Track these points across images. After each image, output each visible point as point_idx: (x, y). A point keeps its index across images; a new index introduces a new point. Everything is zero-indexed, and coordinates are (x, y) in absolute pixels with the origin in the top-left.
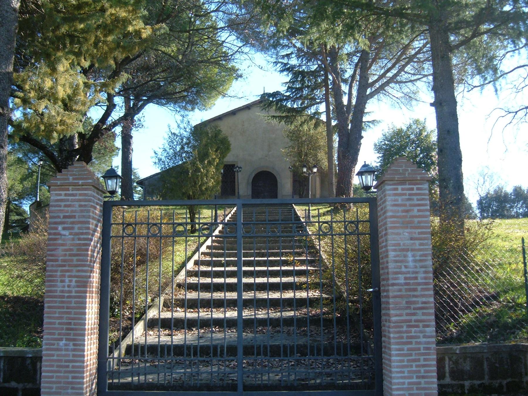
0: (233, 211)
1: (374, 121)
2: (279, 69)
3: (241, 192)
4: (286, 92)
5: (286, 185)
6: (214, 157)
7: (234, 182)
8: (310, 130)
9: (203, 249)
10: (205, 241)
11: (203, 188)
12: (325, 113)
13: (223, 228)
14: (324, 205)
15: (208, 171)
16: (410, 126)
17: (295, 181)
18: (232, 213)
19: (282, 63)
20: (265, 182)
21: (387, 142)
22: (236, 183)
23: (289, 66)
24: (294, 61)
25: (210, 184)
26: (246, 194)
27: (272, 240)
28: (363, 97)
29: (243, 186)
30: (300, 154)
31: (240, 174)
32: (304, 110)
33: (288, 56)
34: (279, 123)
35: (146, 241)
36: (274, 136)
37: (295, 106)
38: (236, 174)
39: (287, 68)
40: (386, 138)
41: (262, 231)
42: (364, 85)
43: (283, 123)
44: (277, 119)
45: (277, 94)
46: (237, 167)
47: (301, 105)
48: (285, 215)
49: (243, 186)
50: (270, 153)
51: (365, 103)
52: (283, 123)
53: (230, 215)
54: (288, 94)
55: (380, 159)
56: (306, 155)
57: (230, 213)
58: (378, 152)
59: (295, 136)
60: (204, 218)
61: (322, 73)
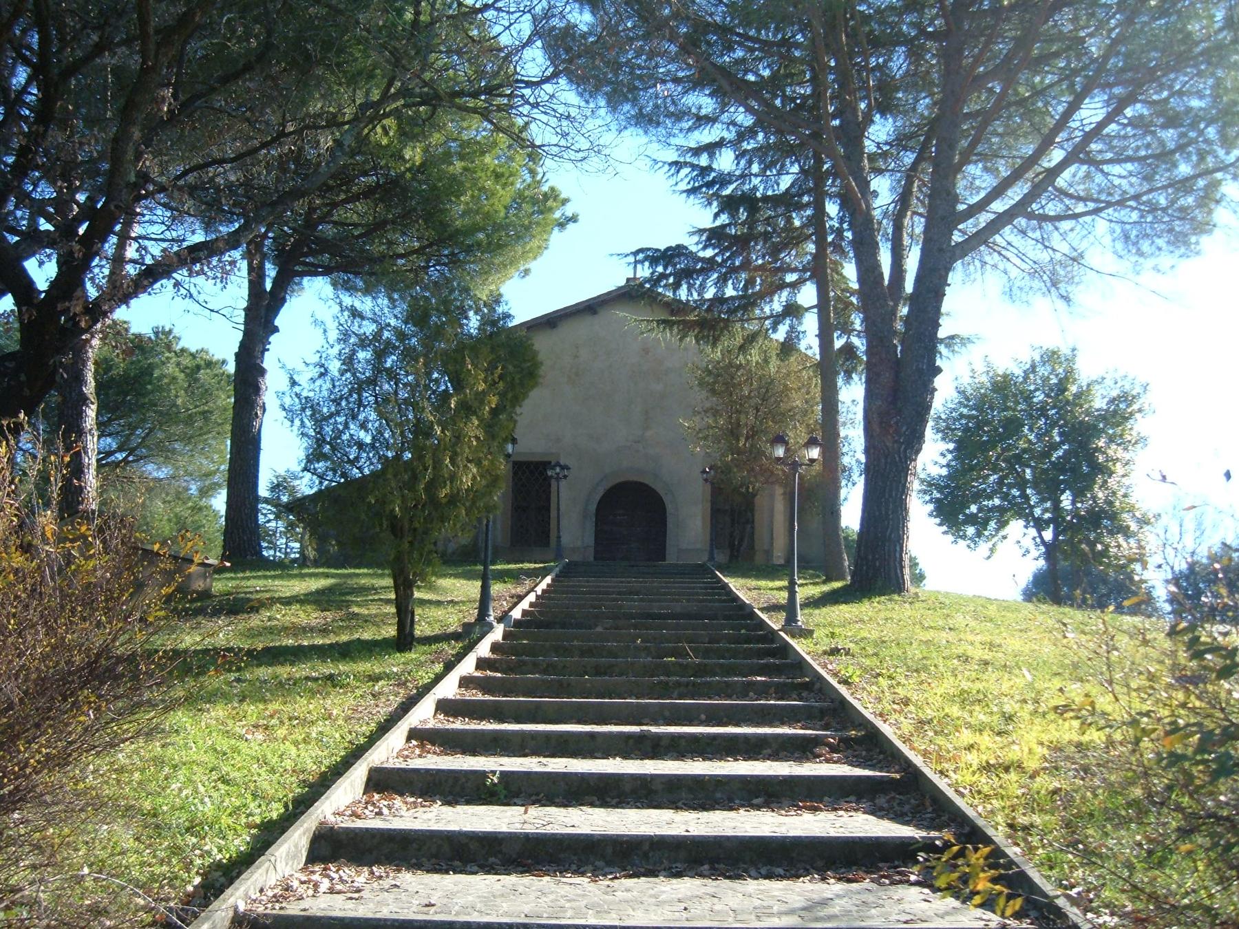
1: (952, 337)
2: (684, 186)
4: (705, 248)
5: (690, 526)
7: (548, 510)
8: (766, 361)
9: (424, 714)
12: (815, 310)
13: (506, 636)
14: (812, 577)
15: (458, 438)
17: (716, 512)
18: (539, 590)
19: (694, 167)
20: (632, 511)
21: (965, 411)
22: (553, 514)
23: (713, 174)
24: (726, 161)
25: (467, 481)
26: (579, 543)
27: (678, 684)
28: (941, 250)
29: (573, 525)
30: (733, 432)
31: (563, 483)
33: (711, 148)
34: (681, 340)
35: (1125, 627)
37: (730, 292)
38: (554, 483)
39: (706, 183)
42: (943, 214)
43: (690, 340)
44: (675, 330)
45: (679, 255)
46: (558, 464)
47: (745, 288)
49: (573, 525)
50: (649, 433)
52: (690, 340)
53: (532, 597)
54: (709, 253)
55: (950, 457)
56: (753, 434)
57: (532, 590)
58: (943, 439)
60: (452, 601)
61: (806, 199)
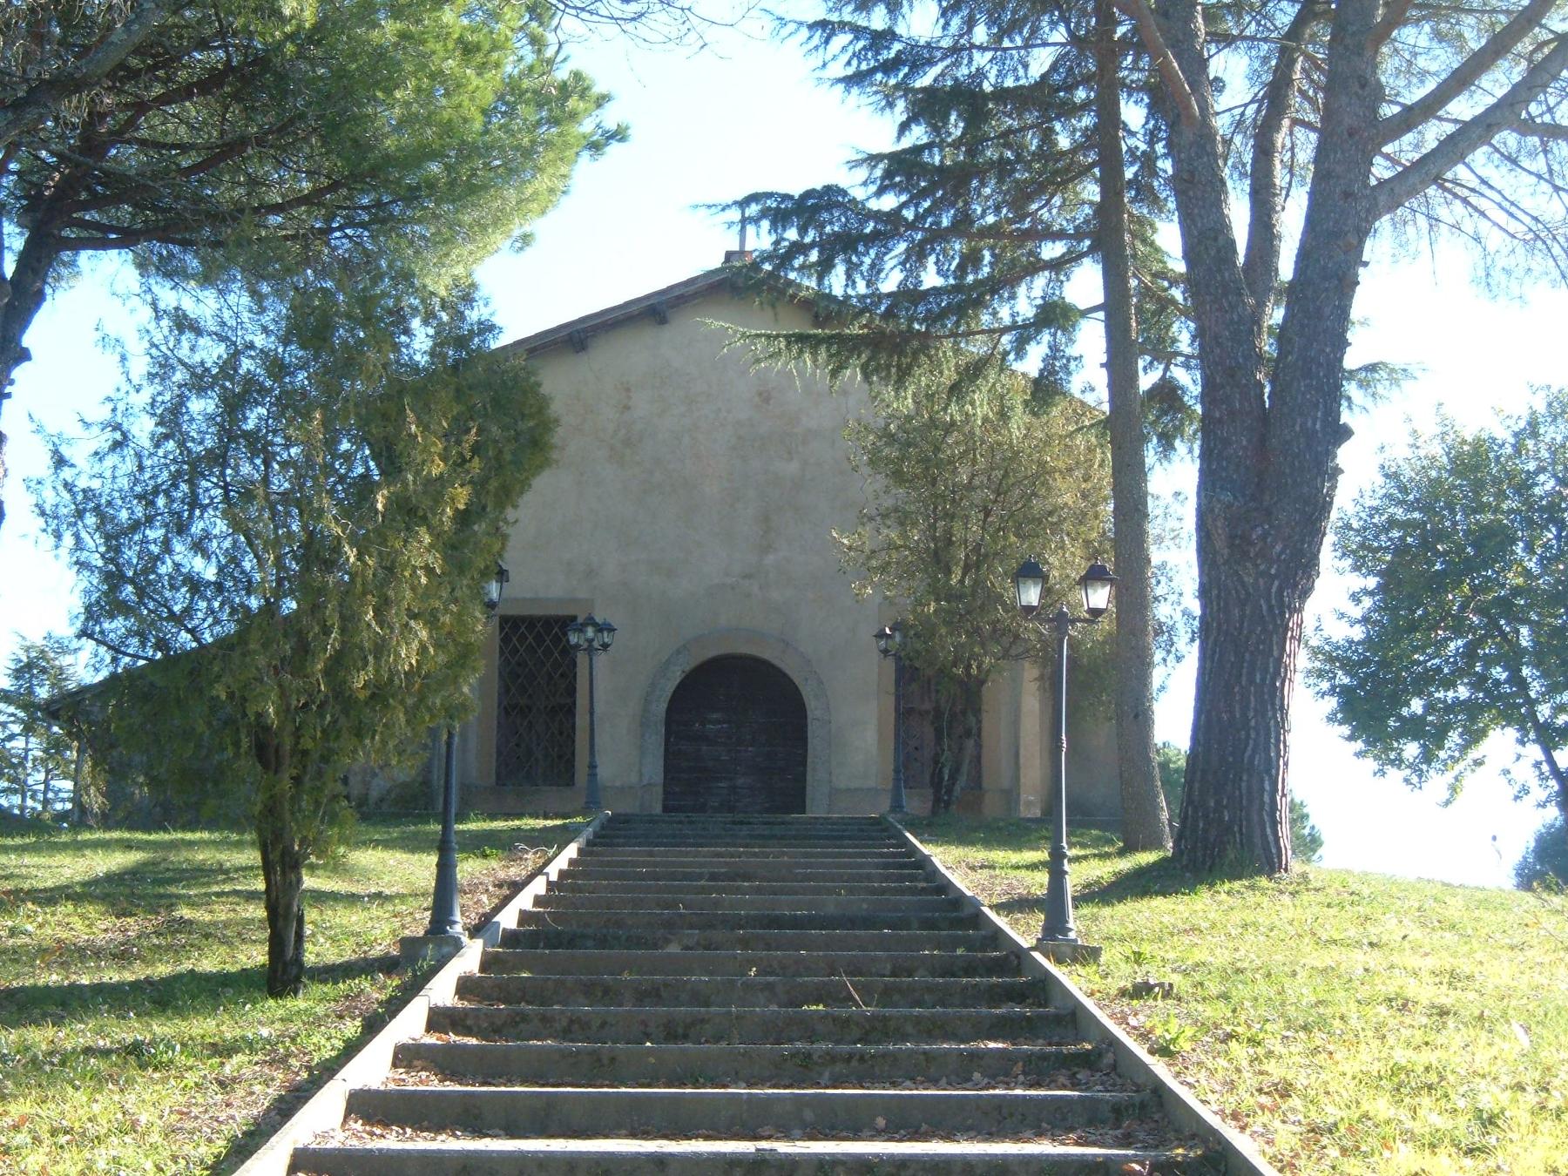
0: (561, 862)
1: (1372, 368)
2: (839, 69)
3: (608, 771)
4: (880, 192)
6: (437, 468)
7: (571, 711)
8: (1003, 415)
10: (351, 1049)
11: (360, 680)
12: (1101, 315)
13: (485, 965)
15: (390, 570)
16: (1533, 428)
18: (553, 871)
19: (858, 31)
20: (738, 715)
21: (1399, 513)
22: (581, 721)
23: (897, 46)
25: (407, 656)
28: (1347, 195)
29: (621, 739)
30: (938, 557)
31: (601, 660)
32: (979, 303)
34: (834, 374)
36: (793, 467)
37: (930, 278)
38: (582, 659)
40: (1403, 489)
41: (748, 986)
42: (1353, 125)
43: (853, 374)
44: (823, 354)
45: (830, 207)
46: (591, 621)
48: (873, 892)
49: (621, 739)
50: (770, 559)
51: (1363, 233)
52: (853, 374)
53: (538, 887)
54: (889, 202)
55: (1367, 602)
56: (979, 560)
57: (539, 871)
58: (1356, 568)
59: (916, 458)
60: (379, 895)
61: (1081, 94)
